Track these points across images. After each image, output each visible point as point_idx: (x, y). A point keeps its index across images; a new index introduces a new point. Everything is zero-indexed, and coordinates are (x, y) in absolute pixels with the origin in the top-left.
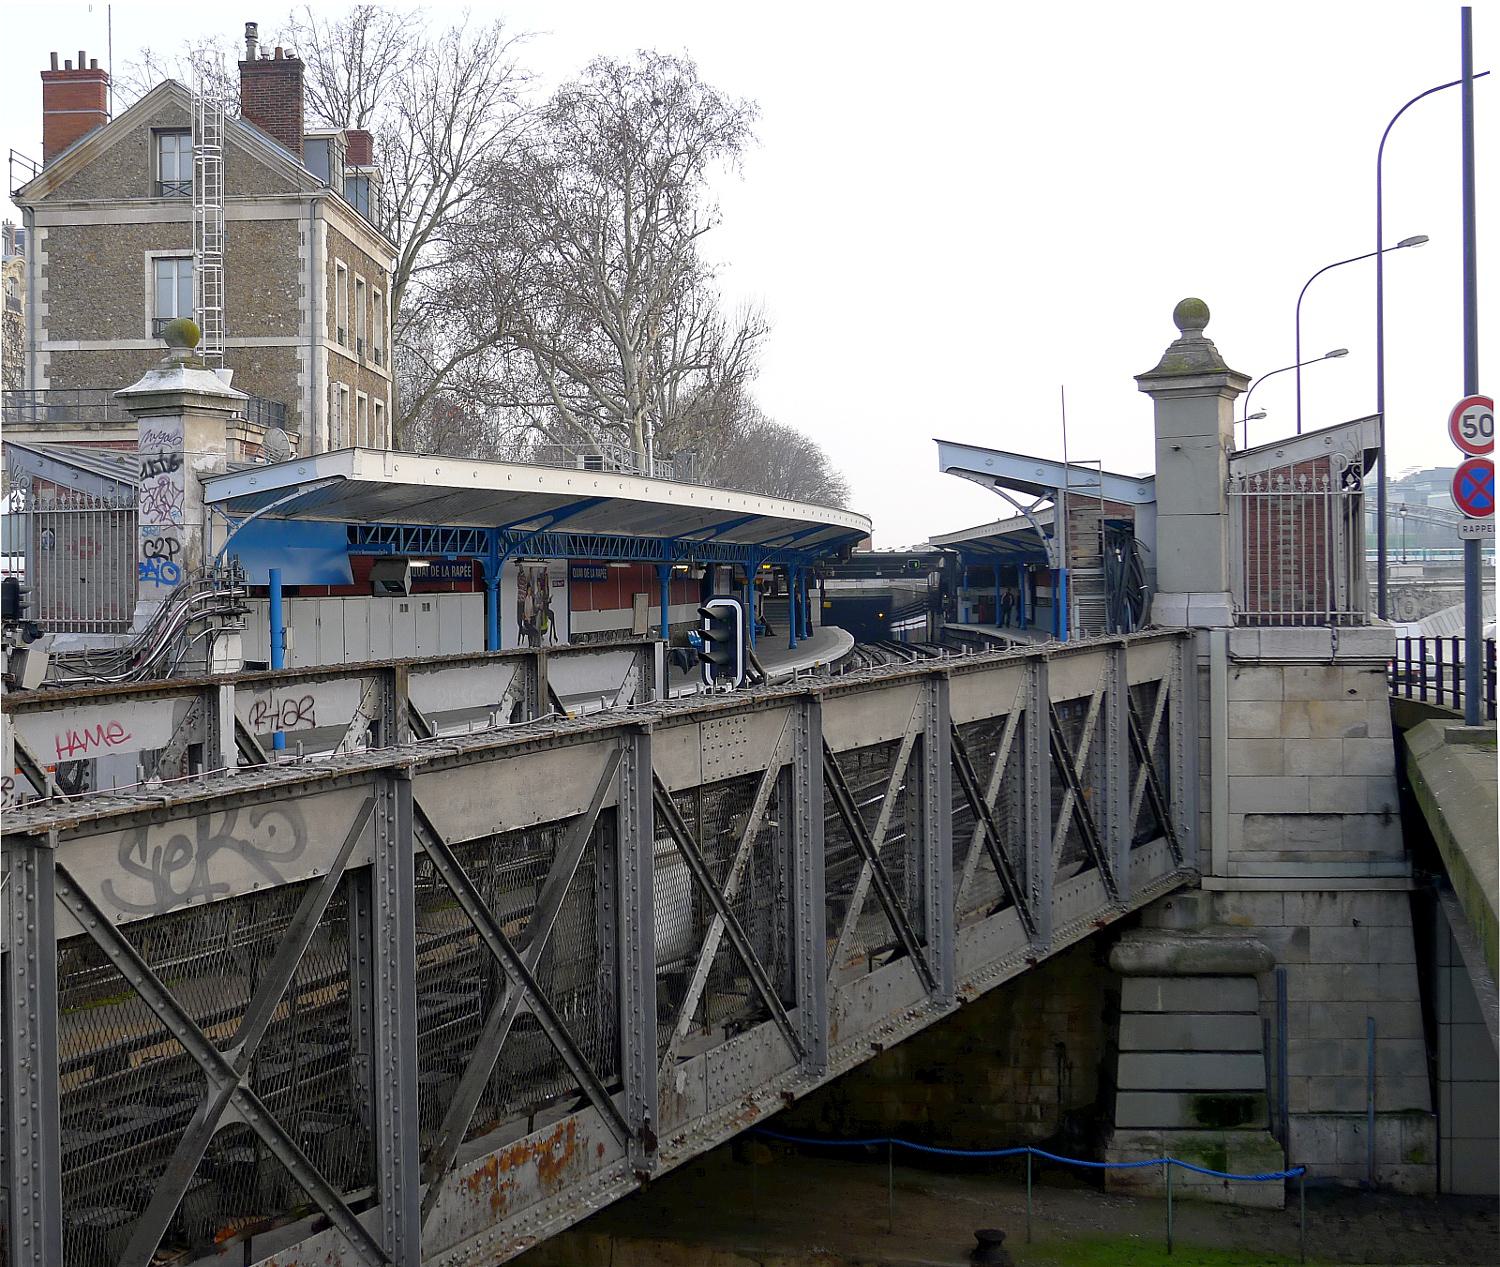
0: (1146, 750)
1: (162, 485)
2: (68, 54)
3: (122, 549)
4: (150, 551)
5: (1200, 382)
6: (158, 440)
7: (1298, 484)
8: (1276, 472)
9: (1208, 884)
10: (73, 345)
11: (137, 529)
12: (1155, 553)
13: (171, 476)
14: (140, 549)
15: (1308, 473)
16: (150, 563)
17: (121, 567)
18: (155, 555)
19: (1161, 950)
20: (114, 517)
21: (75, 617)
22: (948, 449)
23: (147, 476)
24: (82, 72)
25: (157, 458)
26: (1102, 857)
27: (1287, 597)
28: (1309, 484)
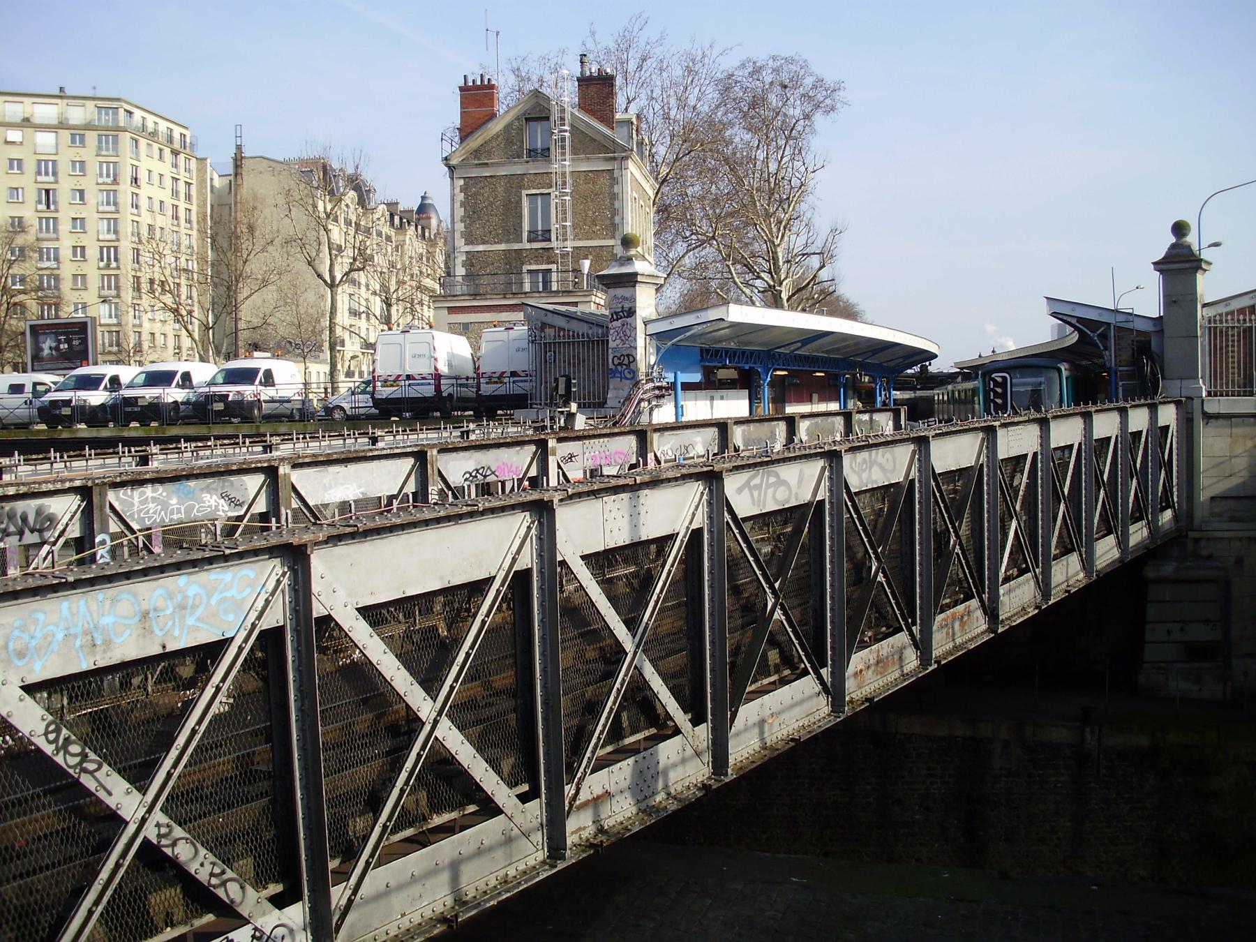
0: (1063, 492)
1: (623, 325)
2: (474, 77)
5: (1187, 265)
7: (1239, 321)
8: (1227, 314)
9: (1192, 535)
10: (481, 248)
11: (607, 350)
12: (1163, 358)
13: (629, 320)
14: (610, 361)
15: (1245, 315)
17: (598, 371)
18: (619, 364)
19: (1169, 569)
20: (593, 344)
21: (584, 399)
22: (1052, 302)
23: (614, 320)
24: (482, 87)
25: (620, 310)
26: (1116, 530)
27: (1233, 381)
28: (1245, 320)
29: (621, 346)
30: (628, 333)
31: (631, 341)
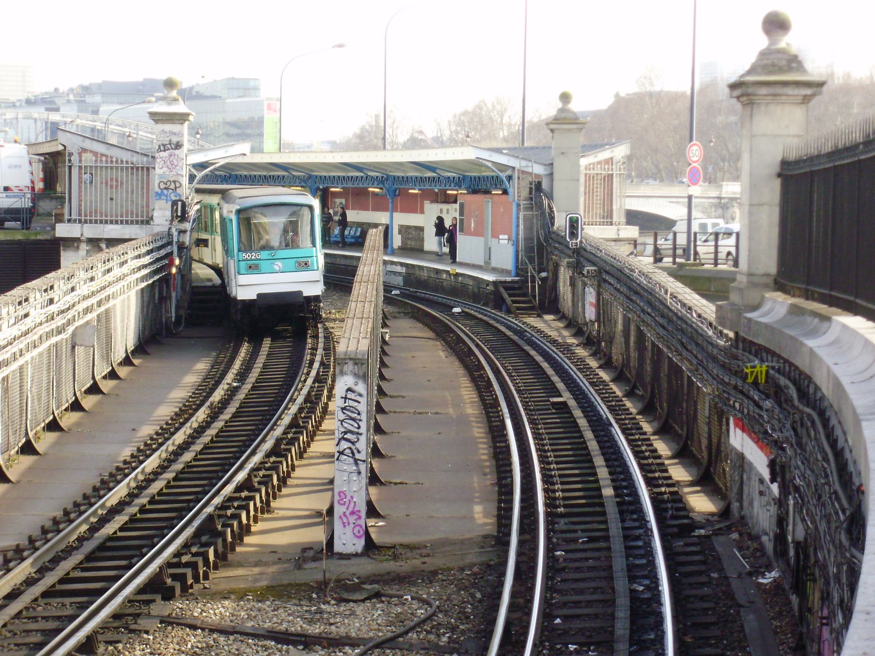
1: (171, 155)
3: (137, 184)
4: (162, 186)
5: (575, 126)
6: (168, 134)
7: (605, 169)
13: (177, 152)
16: (162, 192)
18: (166, 188)
23: (161, 151)
25: (168, 143)
29: (167, 173)
30: (176, 163)
31: (178, 170)
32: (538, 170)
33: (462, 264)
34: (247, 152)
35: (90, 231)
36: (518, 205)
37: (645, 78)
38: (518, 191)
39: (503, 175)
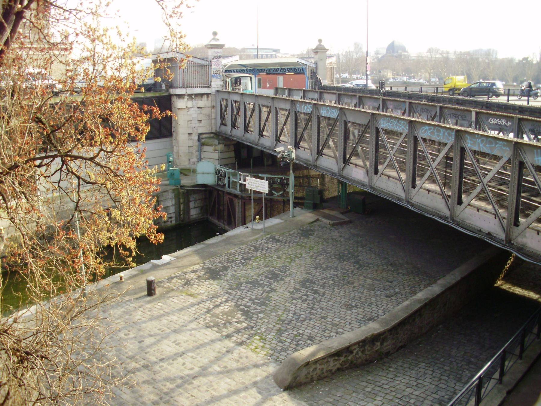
32: (314, 66)
33: (335, 94)
34: (238, 59)
35: (189, 91)
36: (308, 78)
37: (181, 37)
38: (308, 73)
39: (304, 67)
